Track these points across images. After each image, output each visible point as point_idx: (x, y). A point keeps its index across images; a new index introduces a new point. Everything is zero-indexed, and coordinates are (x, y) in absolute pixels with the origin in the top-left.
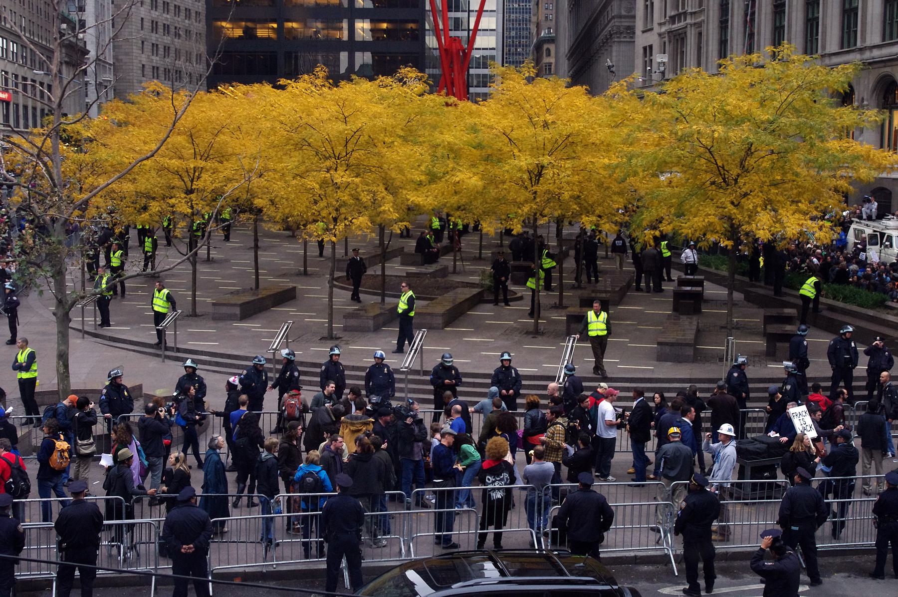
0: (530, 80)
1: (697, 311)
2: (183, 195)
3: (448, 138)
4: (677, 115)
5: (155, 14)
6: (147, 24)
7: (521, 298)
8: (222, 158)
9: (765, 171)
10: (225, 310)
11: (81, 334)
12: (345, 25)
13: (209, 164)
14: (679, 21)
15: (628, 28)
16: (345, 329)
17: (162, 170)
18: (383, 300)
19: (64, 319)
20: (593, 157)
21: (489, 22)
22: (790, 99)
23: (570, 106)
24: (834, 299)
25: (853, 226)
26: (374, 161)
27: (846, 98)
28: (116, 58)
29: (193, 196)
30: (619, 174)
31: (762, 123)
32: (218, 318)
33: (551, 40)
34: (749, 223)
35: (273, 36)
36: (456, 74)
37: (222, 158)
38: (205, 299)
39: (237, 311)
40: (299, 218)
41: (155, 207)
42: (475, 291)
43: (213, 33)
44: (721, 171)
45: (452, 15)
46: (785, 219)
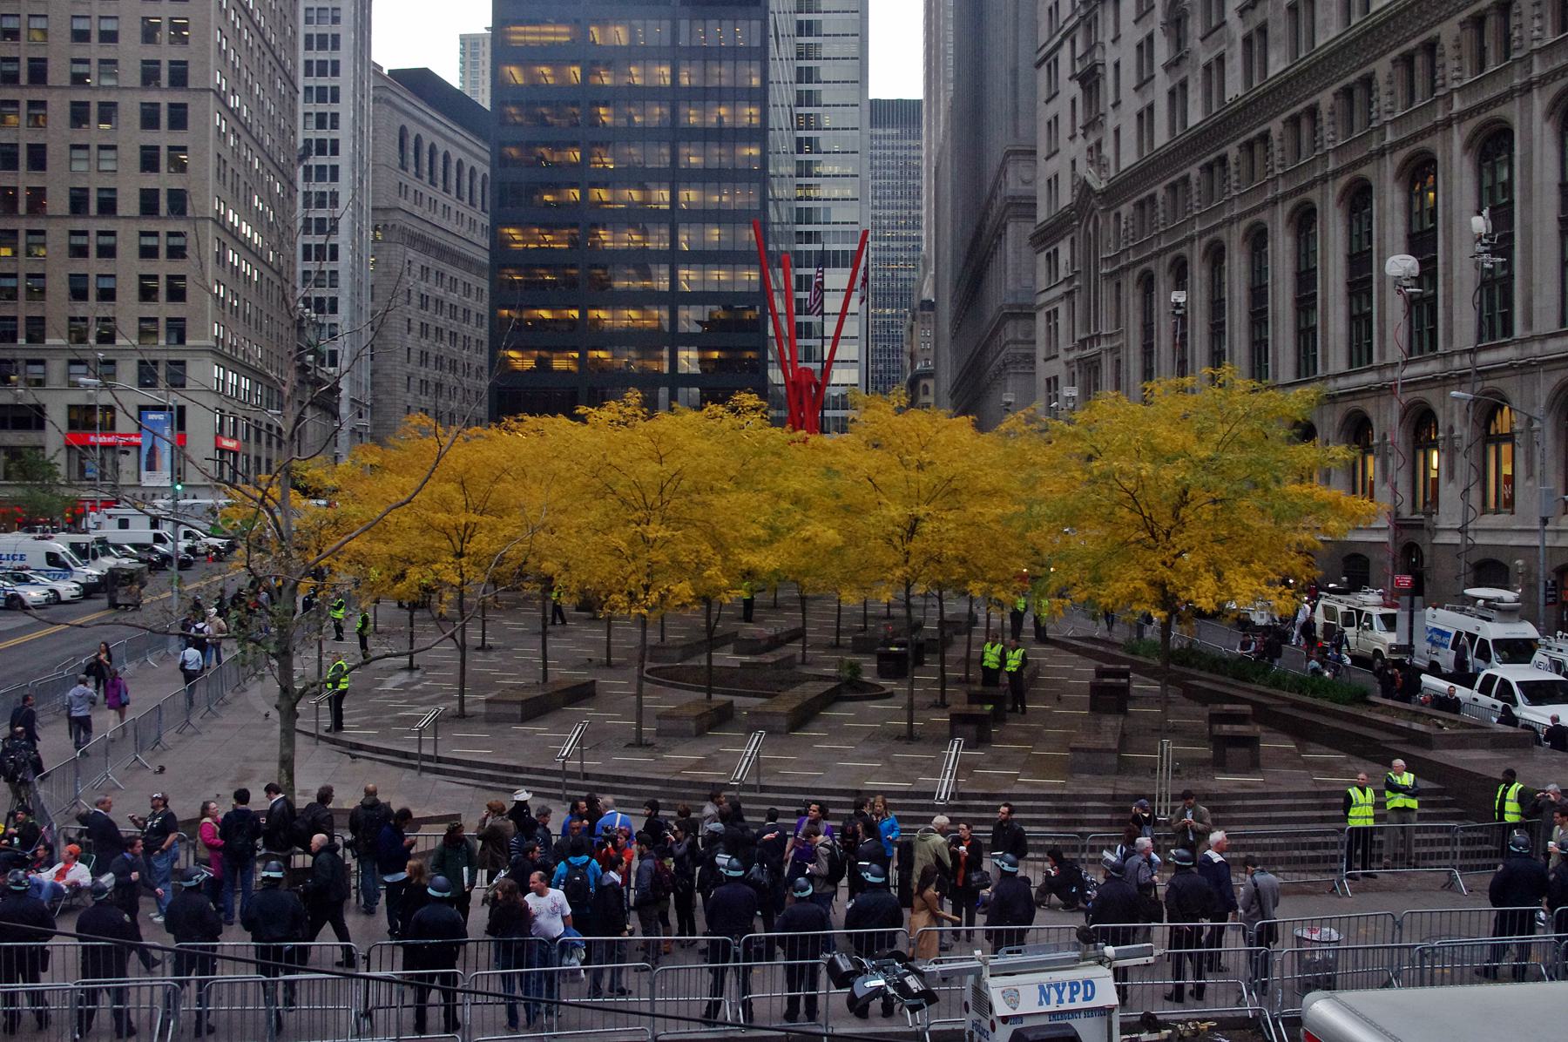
0: (900, 410)
1: (1121, 710)
2: (451, 559)
3: (795, 485)
4: (1092, 451)
5: (425, 343)
6: (415, 356)
7: (890, 695)
8: (501, 511)
9: (1207, 523)
10: (501, 709)
11: (313, 740)
12: (665, 354)
13: (486, 519)
14: (1092, 346)
15: (1027, 356)
16: (659, 733)
17: (428, 528)
18: (709, 697)
19: (289, 714)
20: (982, 506)
21: (846, 351)
22: (1234, 431)
23: (950, 437)
24: (1300, 692)
25: (1322, 602)
26: (699, 513)
27: (1306, 432)
28: (374, 398)
29: (464, 560)
30: (1017, 526)
31: (1202, 461)
32: (492, 719)
33: (929, 375)
34: (1186, 589)
35: (573, 368)
36: (806, 405)
37: (501, 511)
38: (476, 701)
39: (518, 710)
40: (599, 587)
41: (414, 574)
42: (831, 685)
43: (497, 364)
44: (1149, 525)
45: (802, 342)
46: (1233, 584)
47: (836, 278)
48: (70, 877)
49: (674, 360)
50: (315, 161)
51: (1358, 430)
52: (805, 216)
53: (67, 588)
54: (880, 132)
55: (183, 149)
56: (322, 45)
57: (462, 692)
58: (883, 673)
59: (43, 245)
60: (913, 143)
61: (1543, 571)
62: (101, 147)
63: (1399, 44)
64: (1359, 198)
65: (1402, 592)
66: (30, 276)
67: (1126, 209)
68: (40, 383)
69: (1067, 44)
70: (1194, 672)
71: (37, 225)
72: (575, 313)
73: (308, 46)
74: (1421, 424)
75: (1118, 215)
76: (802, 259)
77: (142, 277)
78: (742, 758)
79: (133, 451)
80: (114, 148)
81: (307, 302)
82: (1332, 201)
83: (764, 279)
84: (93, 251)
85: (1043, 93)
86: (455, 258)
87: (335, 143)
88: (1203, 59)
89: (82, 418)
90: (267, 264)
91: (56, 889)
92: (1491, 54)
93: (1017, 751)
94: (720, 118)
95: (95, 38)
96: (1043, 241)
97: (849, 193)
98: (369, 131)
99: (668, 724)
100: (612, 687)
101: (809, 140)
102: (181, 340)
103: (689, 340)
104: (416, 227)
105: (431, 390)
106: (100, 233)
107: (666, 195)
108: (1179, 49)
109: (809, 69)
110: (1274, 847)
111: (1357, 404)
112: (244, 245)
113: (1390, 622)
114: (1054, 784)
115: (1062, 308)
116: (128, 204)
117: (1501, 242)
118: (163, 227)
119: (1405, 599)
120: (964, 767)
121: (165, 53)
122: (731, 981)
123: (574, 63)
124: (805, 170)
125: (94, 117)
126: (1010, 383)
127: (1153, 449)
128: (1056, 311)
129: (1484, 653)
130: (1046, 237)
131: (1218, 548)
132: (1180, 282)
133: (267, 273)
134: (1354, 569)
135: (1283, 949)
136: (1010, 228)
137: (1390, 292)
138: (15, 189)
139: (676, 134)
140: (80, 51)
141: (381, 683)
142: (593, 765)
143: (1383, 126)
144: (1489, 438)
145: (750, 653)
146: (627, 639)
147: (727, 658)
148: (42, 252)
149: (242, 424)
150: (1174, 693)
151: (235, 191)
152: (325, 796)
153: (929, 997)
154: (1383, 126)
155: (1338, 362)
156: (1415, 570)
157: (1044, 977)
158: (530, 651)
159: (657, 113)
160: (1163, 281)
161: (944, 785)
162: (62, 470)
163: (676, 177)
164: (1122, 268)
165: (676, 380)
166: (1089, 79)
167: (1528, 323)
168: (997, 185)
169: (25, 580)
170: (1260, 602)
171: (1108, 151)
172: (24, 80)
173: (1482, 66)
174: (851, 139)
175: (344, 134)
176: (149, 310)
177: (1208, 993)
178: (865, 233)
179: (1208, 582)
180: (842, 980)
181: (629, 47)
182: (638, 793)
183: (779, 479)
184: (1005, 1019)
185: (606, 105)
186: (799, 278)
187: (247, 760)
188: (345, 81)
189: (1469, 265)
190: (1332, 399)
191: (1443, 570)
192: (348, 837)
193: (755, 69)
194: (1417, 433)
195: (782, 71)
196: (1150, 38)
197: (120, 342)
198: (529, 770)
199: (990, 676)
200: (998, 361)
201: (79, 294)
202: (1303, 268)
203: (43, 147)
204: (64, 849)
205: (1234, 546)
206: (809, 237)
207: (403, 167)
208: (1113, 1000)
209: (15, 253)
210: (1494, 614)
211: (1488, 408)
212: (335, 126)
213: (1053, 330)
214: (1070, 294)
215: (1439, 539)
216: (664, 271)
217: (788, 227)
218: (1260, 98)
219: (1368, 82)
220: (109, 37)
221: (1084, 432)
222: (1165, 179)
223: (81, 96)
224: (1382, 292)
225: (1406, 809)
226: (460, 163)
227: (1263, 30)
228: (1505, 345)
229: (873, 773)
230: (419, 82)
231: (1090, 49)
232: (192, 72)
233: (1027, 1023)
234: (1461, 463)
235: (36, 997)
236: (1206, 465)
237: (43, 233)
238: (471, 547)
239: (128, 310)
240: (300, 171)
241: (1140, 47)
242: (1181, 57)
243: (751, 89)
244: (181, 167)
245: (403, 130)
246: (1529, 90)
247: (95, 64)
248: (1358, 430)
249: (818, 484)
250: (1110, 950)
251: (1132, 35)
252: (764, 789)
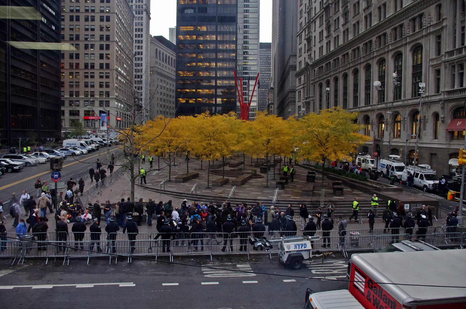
0: (266, 115)
1: (313, 181)
3: (243, 131)
5: (161, 96)
7: (263, 177)
8: (179, 136)
12: (214, 99)
13: (176, 138)
16: (212, 186)
19: (133, 182)
21: (254, 99)
23: (278, 122)
25: (358, 157)
26: (221, 138)
27: (355, 121)
28: (150, 108)
32: (176, 182)
33: (272, 104)
35: (194, 102)
36: (245, 113)
37: (179, 136)
38: (173, 177)
39: (182, 180)
41: (160, 150)
43: (177, 101)
44: (320, 142)
45: (244, 97)
47: (252, 83)
48: (87, 217)
49: (216, 101)
50: (137, 56)
51: (367, 120)
52: (245, 69)
53: (85, 151)
54: (262, 50)
55: (109, 54)
56: (139, 31)
57: (170, 175)
58: (261, 172)
59: (79, 75)
60: (269, 52)
61: (406, 151)
62: (91, 54)
63: (378, 34)
64: (368, 68)
65: (375, 156)
66: (76, 82)
67: (316, 69)
68: (78, 106)
69: (304, 32)
70: (329, 173)
71: (77, 71)
72: (194, 90)
73: (136, 31)
74: (381, 118)
75: (315, 70)
76: (244, 78)
77: (100, 82)
78: (231, 192)
79: (98, 121)
80: (94, 54)
81: (136, 87)
82: (362, 68)
83: (236, 83)
84: (89, 77)
85: (298, 43)
86: (168, 78)
87: (142, 52)
88: (334, 36)
89: (87, 113)
90: (127, 79)
91: (84, 220)
92: (398, 36)
93: (290, 190)
94: (227, 47)
95: (90, 30)
97: (255, 64)
98: (149, 49)
99: (215, 184)
100: (202, 174)
101: (246, 52)
102: (109, 96)
103: (219, 96)
104: (159, 71)
105: (163, 106)
106: (91, 73)
107: (214, 64)
108: (329, 33)
109: (246, 36)
110: (346, 213)
111: (366, 113)
112: (122, 75)
113: (372, 162)
114: (298, 198)
115: (302, 90)
116: (97, 66)
117: (399, 79)
118: (104, 71)
119: (376, 158)
120: (279, 194)
121: (105, 33)
122: (228, 243)
123: (195, 35)
124: (245, 58)
125: (89, 47)
126: (290, 106)
127: (322, 125)
129: (393, 169)
130: (298, 75)
131: (335, 147)
132: (328, 86)
133: (127, 81)
134: (365, 150)
135: (347, 237)
137: (375, 89)
138: (73, 63)
139: (217, 51)
140: (87, 33)
141: (152, 173)
142: (198, 192)
143: (374, 52)
144: (395, 121)
145: (232, 167)
146: (205, 164)
147: (227, 168)
148: (79, 77)
149: (122, 114)
150: (325, 177)
151: (120, 63)
152: (141, 200)
153: (271, 247)
154: (374, 52)
155: (362, 104)
156: (378, 151)
157: (296, 243)
158: (185, 166)
159: (213, 46)
160: (324, 85)
161: (275, 198)
162: (83, 125)
163: (217, 60)
165: (216, 105)
166: (309, 40)
167: (405, 96)
168: (288, 62)
169: (76, 149)
170: (343, 157)
171: (313, 56)
172: (74, 39)
173: (396, 39)
174: (255, 52)
175: (144, 50)
176: (101, 90)
177: (331, 245)
179: (333, 155)
180: (253, 243)
181: (206, 31)
182: (208, 199)
183: (239, 130)
184: (287, 252)
185: (201, 44)
186: (244, 82)
187: (124, 190)
188: (144, 39)
189: (392, 83)
190: (362, 112)
191: (385, 151)
192: (146, 209)
193: (234, 36)
194: (379, 120)
195: (240, 36)
196: (322, 31)
197: (96, 97)
198: (184, 194)
199: (285, 173)
200: (287, 102)
201: (86, 86)
203: (79, 54)
204: (86, 211)
205: (340, 147)
207: (157, 57)
208: (310, 248)
209: (73, 77)
210: (395, 161)
211: (396, 115)
212: (142, 49)
213: (300, 96)
214: (304, 87)
215: (384, 144)
216: (214, 81)
218: (347, 45)
219: (371, 42)
220: (93, 30)
221: (306, 121)
222: (391, 26)
223: (87, 43)
224: (373, 89)
225: (376, 205)
226: (169, 57)
227: (347, 30)
228: (399, 101)
229: (258, 195)
230: (160, 39)
231: (309, 33)
232: (111, 37)
233: (292, 253)
234: (389, 128)
235: (81, 244)
236: (334, 129)
237: (79, 73)
238: (172, 144)
239: (97, 89)
240: (134, 59)
241: (320, 33)
242: (329, 35)
243: (233, 41)
244: (108, 58)
245: (156, 50)
246: (406, 45)
247: (90, 35)
248: (367, 120)
249: (248, 131)
250: (310, 237)
251: (318, 30)
252: (235, 198)
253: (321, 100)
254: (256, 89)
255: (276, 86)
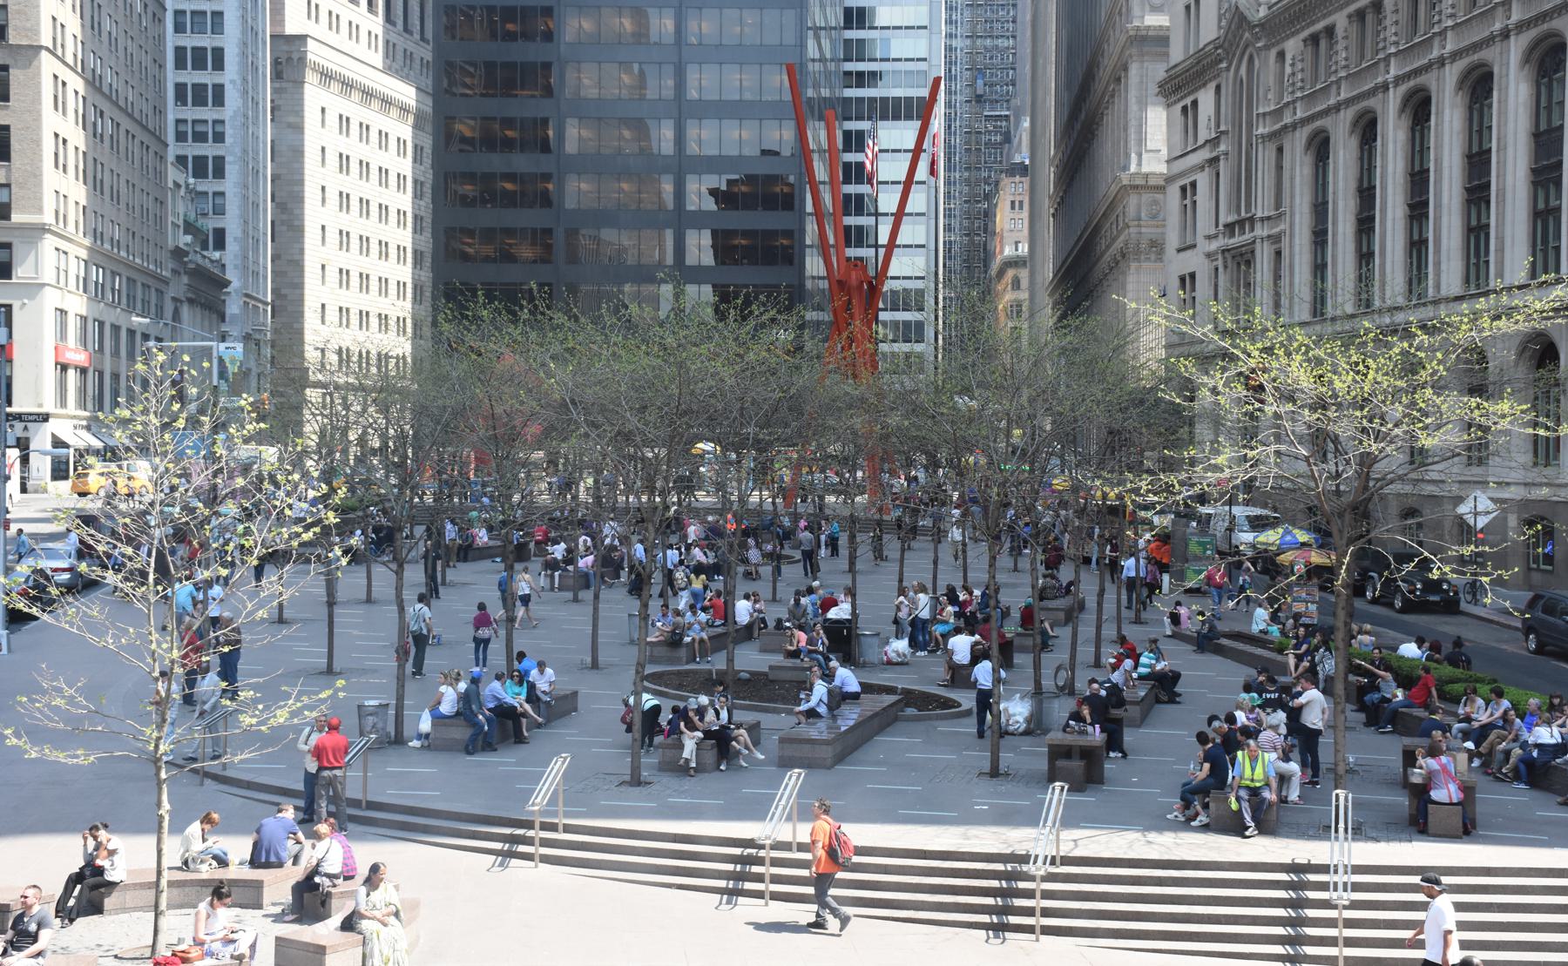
56: (199, 64)
67: (1293, 46)
75: (1281, 55)
76: (849, 109)
96: (1178, 88)
107: (669, 24)
115: (1203, 180)
128: (1194, 185)
136: (1134, 69)
154: (1443, 33)
164: (1285, 127)
178: (937, 81)
186: (847, 135)
202: (1475, 149)
206: (861, 79)
214: (1214, 161)
217: (832, 66)
246: (1443, 65)
253: (1320, 237)
254: (922, 172)
255: (1050, 148)
